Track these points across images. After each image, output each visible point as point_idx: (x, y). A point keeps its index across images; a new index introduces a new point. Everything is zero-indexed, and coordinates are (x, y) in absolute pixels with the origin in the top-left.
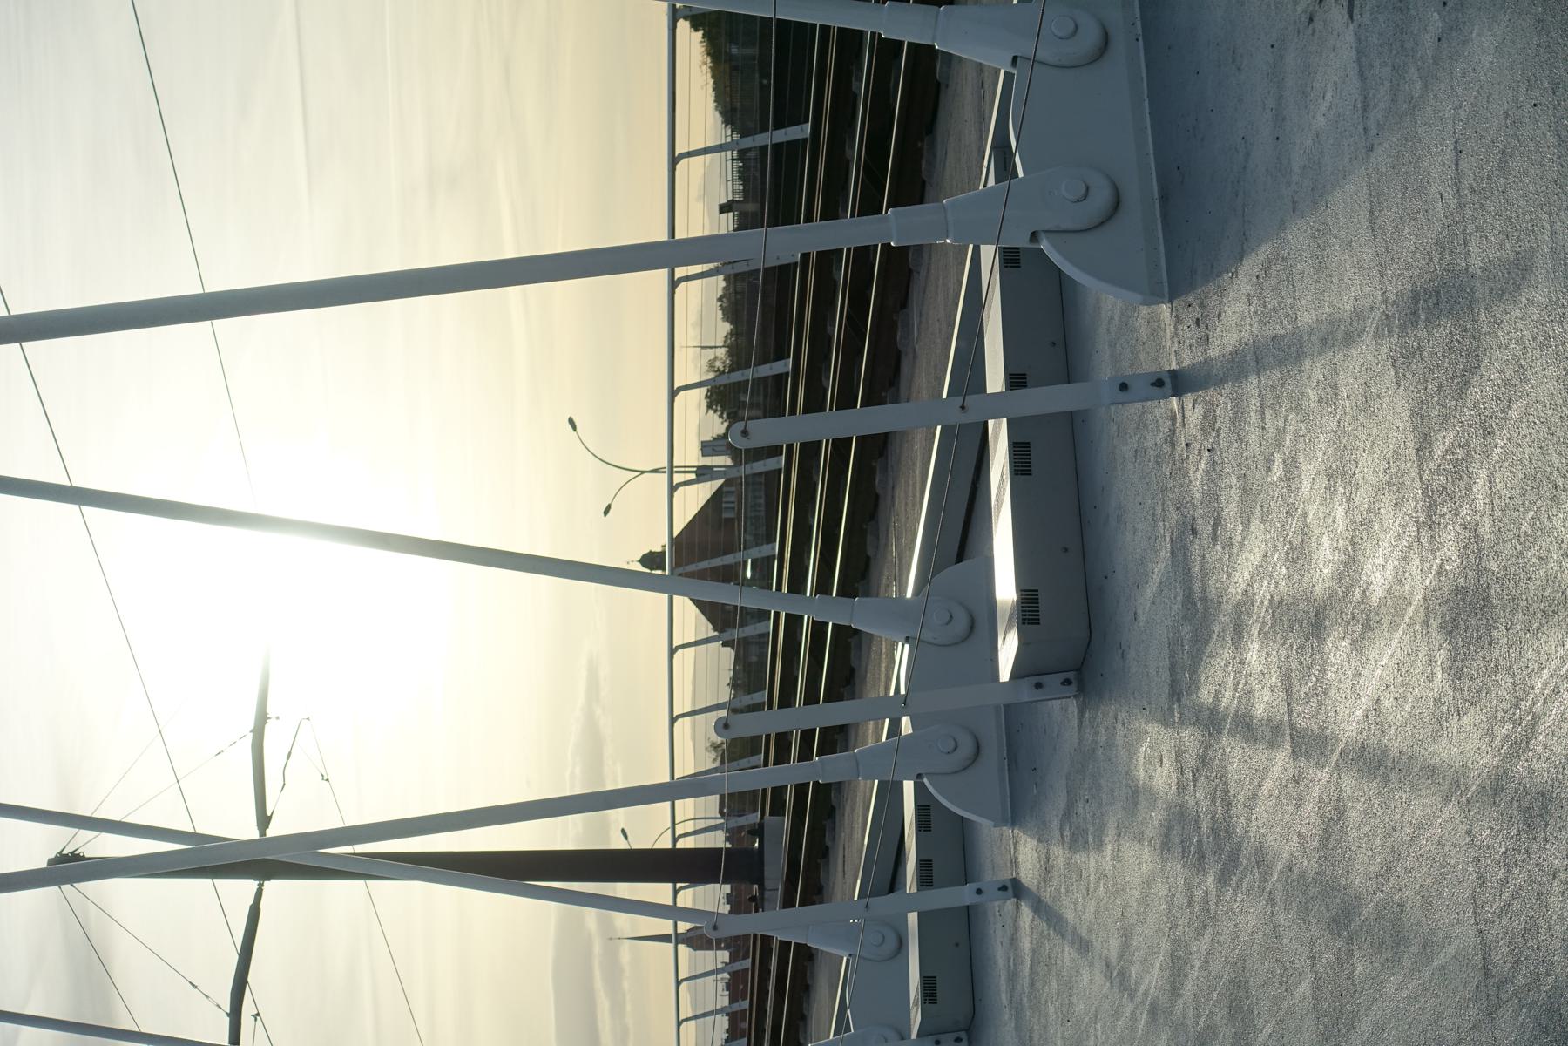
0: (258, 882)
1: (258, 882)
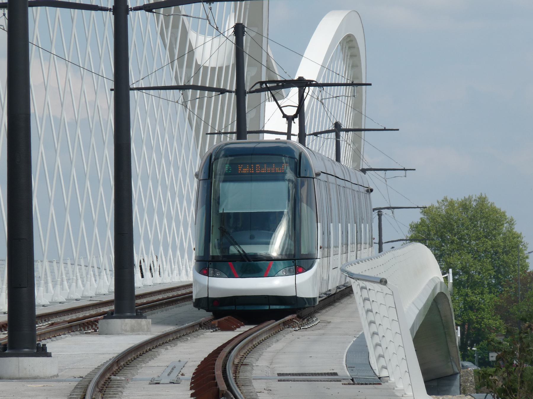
0: (112, 8)
1: (112, 8)
